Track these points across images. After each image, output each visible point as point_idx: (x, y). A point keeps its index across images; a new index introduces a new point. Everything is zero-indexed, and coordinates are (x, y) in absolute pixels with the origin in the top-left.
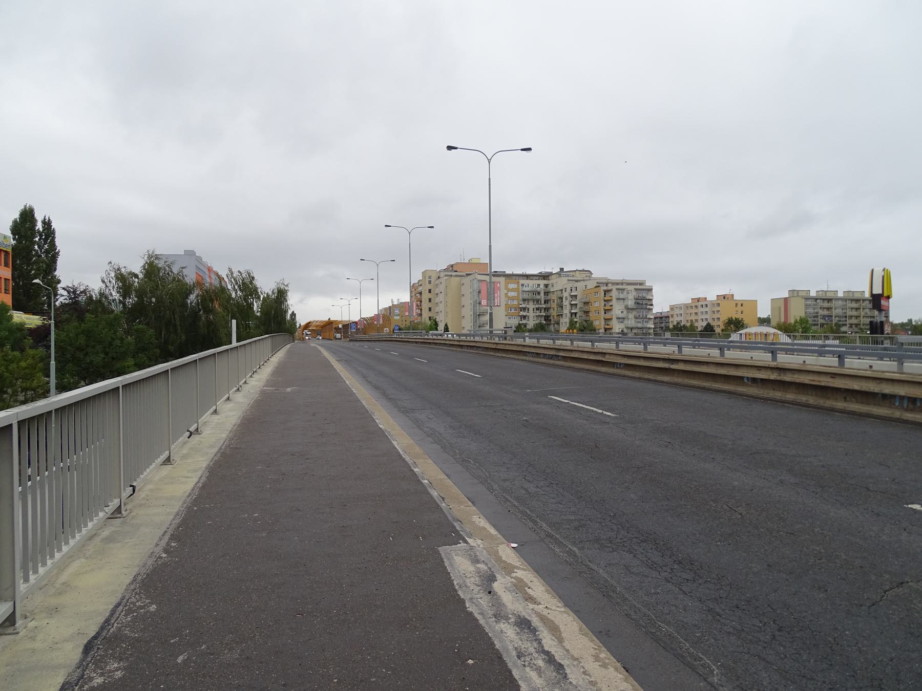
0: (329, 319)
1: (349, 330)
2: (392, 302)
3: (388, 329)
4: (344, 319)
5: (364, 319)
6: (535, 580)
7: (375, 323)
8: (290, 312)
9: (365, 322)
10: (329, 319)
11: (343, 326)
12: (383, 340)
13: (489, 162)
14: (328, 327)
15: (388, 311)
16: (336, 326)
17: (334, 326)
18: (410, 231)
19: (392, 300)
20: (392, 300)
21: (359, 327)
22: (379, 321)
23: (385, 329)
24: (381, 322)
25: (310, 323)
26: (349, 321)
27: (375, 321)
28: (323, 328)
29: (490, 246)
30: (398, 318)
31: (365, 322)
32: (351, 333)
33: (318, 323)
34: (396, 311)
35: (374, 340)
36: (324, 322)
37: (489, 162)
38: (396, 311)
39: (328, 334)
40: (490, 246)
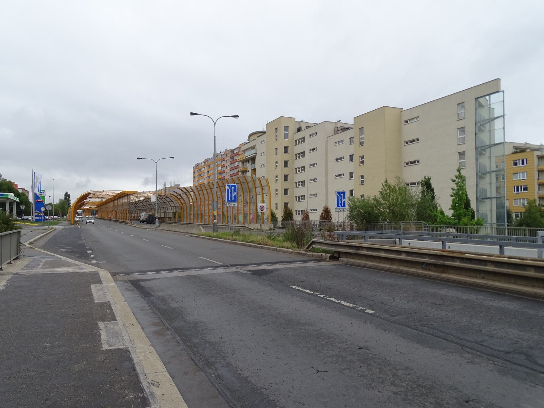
18: (215, 121)
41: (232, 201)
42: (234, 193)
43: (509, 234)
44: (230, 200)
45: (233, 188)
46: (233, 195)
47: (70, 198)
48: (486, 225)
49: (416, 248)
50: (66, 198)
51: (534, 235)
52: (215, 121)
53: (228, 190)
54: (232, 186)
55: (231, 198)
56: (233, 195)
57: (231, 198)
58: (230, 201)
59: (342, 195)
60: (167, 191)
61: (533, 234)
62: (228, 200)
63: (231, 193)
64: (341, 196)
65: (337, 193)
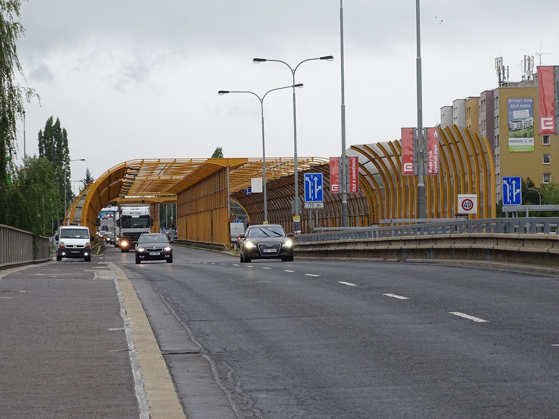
0: (218, 153)
1: (295, 203)
2: (501, 70)
3: (474, 197)
4: (272, 154)
5: (365, 150)
6: (145, 214)
7: (408, 167)
8: (62, 129)
9: (370, 166)
10: (218, 153)
11: (271, 186)
12: (438, 252)
13: (262, 102)
14: (204, 189)
15: (483, 116)
16: (239, 187)
17: (231, 190)
18: (261, 98)
19: (499, 60)
20: (499, 60)
21: (334, 188)
22: (422, 157)
23: (462, 197)
24: (434, 164)
25: (121, 172)
26: (296, 161)
27: (407, 159)
28: (188, 196)
29: (343, 108)
30: (527, 144)
31: (370, 166)
32: (305, 216)
33: (159, 175)
34: (516, 115)
35: (400, 251)
36: (189, 165)
37: (262, 102)
38: (516, 115)
39: (204, 220)
40: (343, 108)
41: (315, 199)
42: (317, 188)
43: (16, 260)
44: (310, 198)
45: (316, 179)
46: (316, 190)
47: (66, 145)
48: (69, 255)
49: (428, 262)
50: (49, 147)
51: (10, 261)
52: (262, 98)
53: (307, 182)
54: (314, 176)
55: (313, 195)
56: (316, 190)
57: (313, 195)
58: (311, 200)
59: (514, 182)
60: (497, 104)
61: (15, 260)
62: (308, 199)
63: (313, 187)
64: (512, 185)
65: (504, 179)
